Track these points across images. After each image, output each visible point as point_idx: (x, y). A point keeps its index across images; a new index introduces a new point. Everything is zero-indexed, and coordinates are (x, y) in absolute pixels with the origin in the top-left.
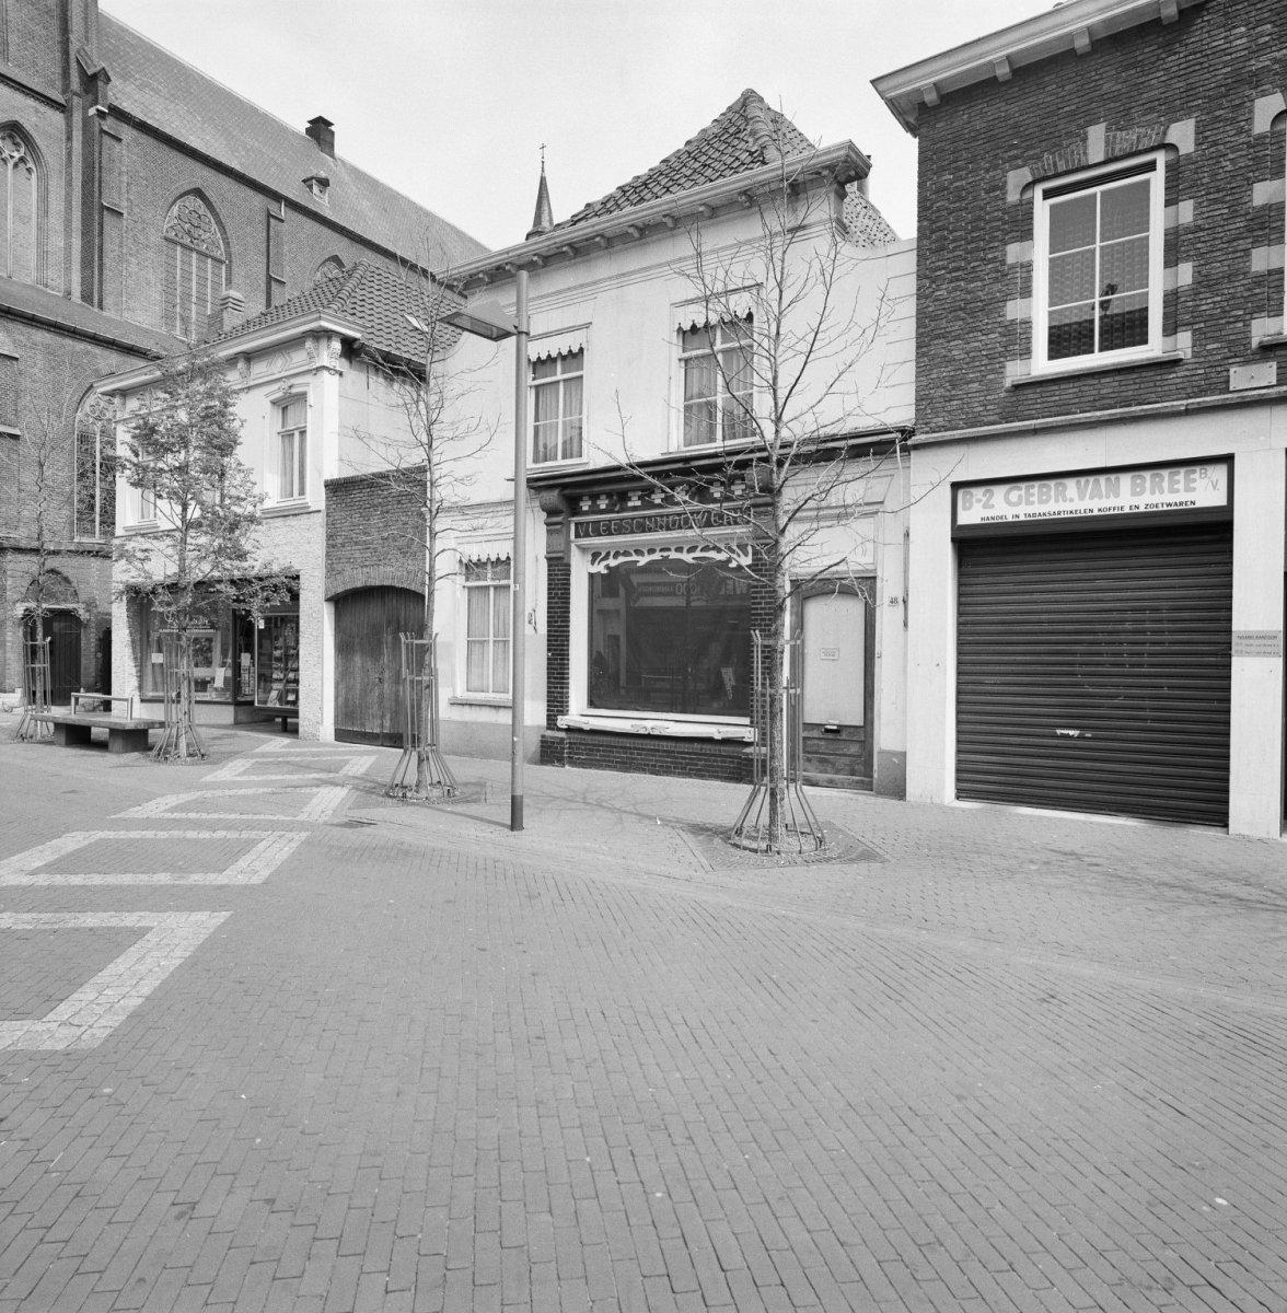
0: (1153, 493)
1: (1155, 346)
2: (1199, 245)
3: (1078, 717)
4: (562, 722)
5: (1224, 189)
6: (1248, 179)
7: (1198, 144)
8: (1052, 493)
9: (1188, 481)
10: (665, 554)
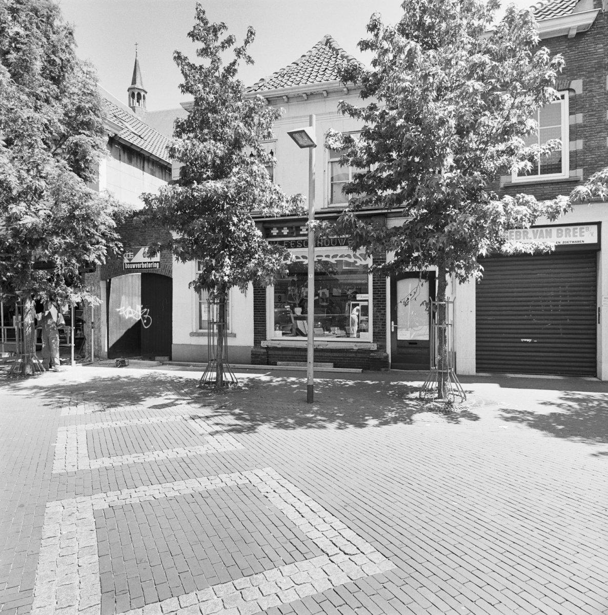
0: (566, 236)
1: (566, 173)
2: (585, 133)
3: (533, 334)
4: (264, 344)
5: (595, 111)
6: (605, 108)
7: (584, 90)
8: (522, 235)
9: (581, 232)
10: (320, 258)
